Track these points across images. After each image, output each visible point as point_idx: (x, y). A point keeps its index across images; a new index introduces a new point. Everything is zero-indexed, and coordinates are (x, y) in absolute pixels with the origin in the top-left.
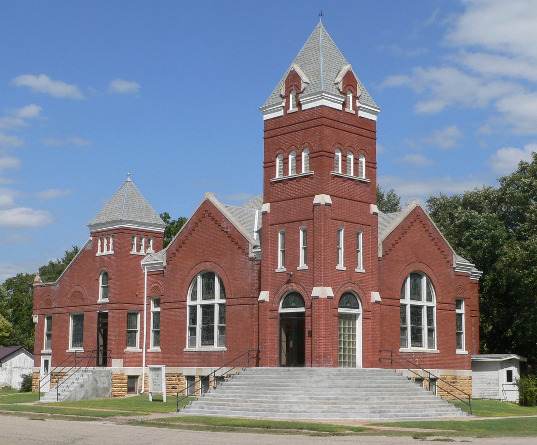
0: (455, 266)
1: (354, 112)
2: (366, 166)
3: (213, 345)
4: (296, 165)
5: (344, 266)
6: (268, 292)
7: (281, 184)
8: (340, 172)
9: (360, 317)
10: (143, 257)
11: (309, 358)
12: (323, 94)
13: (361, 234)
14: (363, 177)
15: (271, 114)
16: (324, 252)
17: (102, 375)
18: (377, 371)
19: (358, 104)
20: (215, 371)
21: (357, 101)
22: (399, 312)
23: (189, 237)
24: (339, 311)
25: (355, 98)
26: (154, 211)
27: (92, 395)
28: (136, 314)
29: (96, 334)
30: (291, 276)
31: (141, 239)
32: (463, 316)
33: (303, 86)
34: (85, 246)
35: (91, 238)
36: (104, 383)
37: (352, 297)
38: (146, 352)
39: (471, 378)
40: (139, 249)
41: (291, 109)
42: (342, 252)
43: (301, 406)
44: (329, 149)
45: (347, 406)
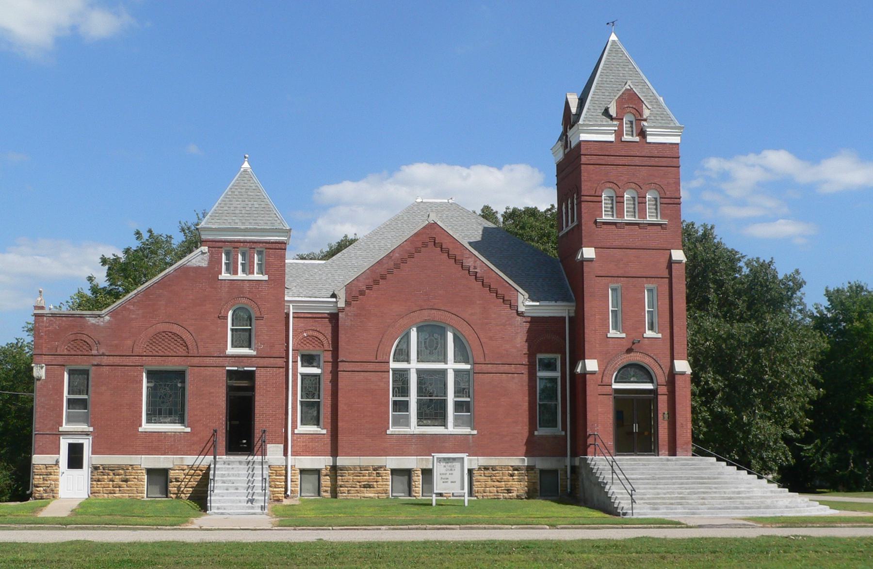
11: (664, 445)
38: (293, 433)
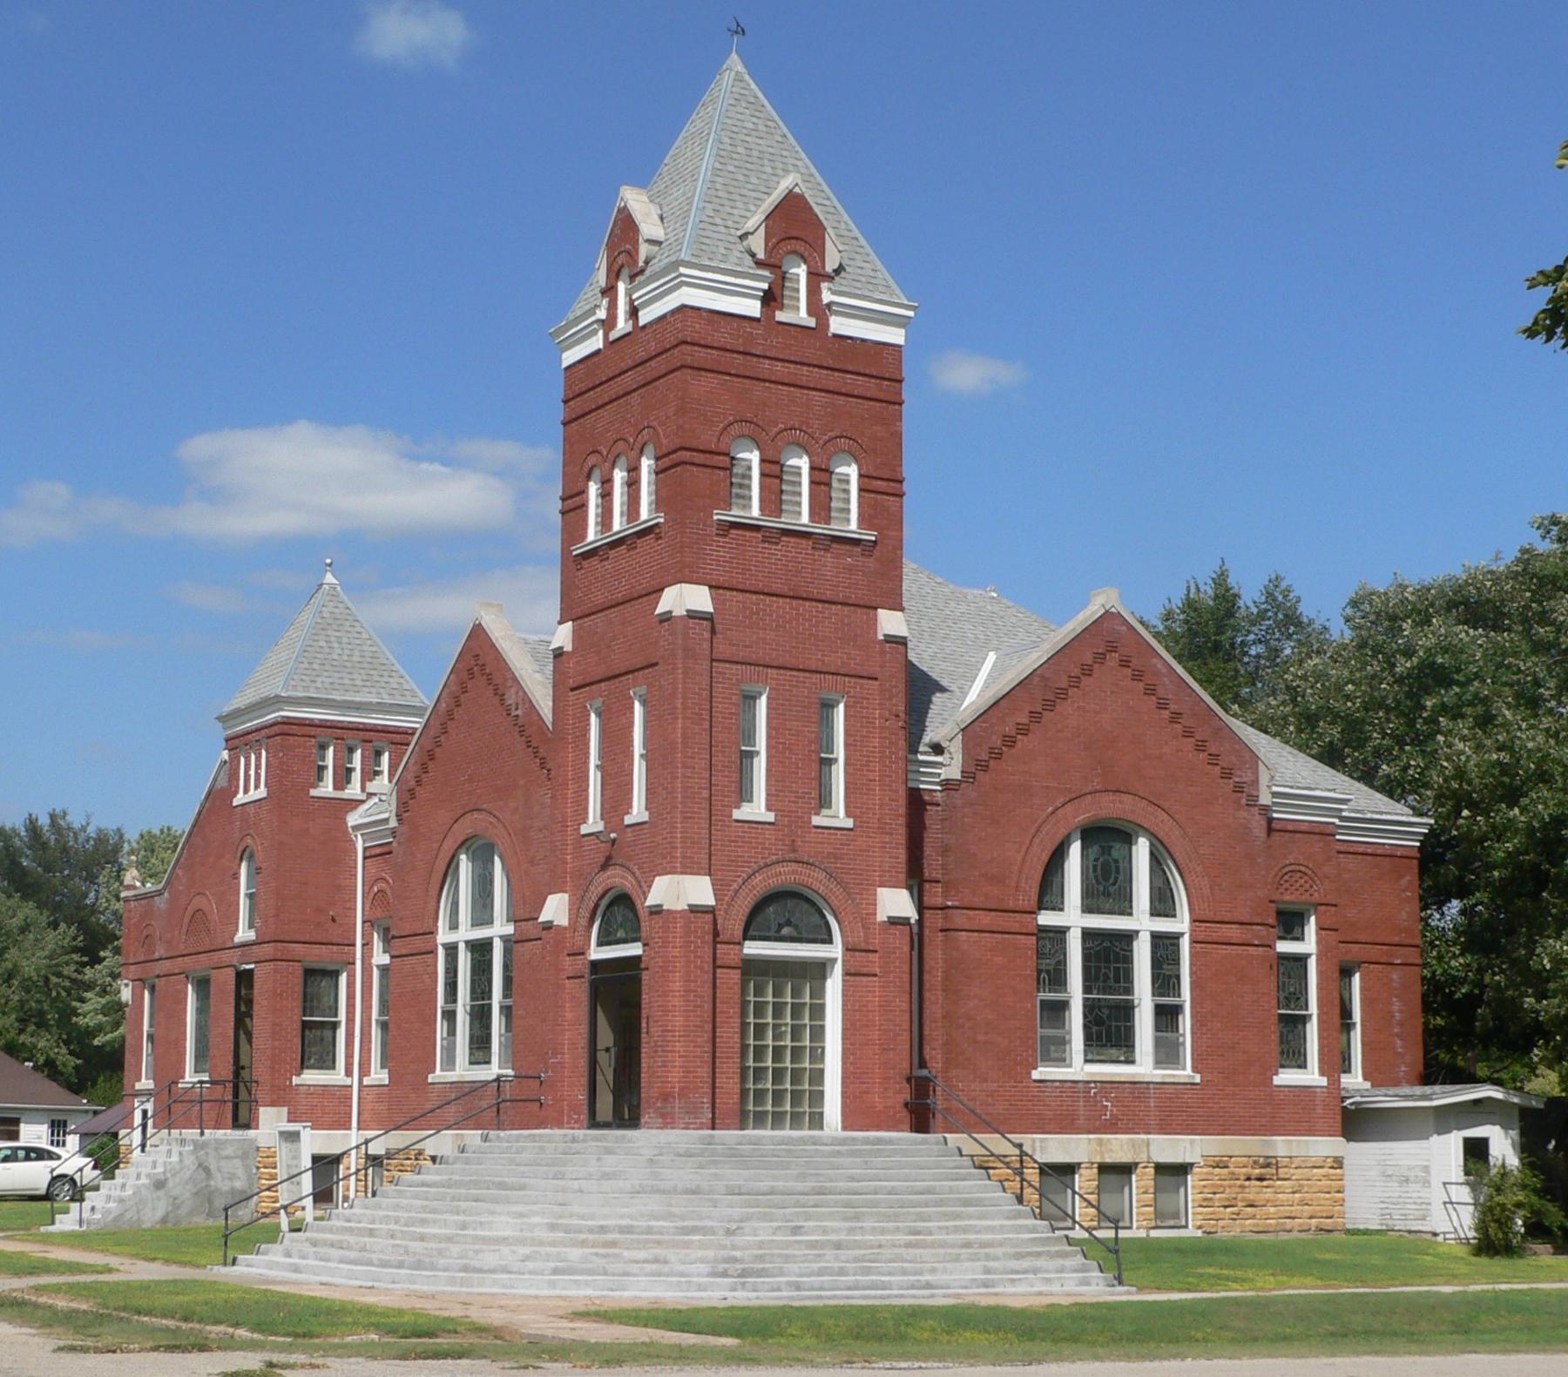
0: (1265, 799)
1: (812, 323)
2: (861, 490)
3: (488, 1062)
4: (629, 498)
5: (769, 808)
6: (566, 896)
7: (594, 561)
8: (755, 511)
9: (838, 969)
10: (354, 804)
12: (683, 270)
13: (841, 706)
14: (852, 526)
15: (577, 348)
16: (685, 767)
17: (225, 1153)
18: (866, 1141)
19: (827, 297)
20: (367, 1142)
21: (824, 285)
22: (1032, 953)
23: (443, 738)
24: (746, 951)
25: (816, 277)
26: (397, 666)
27: (191, 1213)
28: (335, 975)
29: (231, 1033)
30: (614, 841)
31: (351, 750)
32: (1312, 964)
33: (644, 250)
34: (215, 779)
35: (225, 755)
36: (232, 1177)
37: (806, 906)
39: (1338, 1163)
40: (342, 778)
41: (622, 325)
42: (760, 766)
43: (505, 1250)
44: (708, 439)
45: (642, 1255)
